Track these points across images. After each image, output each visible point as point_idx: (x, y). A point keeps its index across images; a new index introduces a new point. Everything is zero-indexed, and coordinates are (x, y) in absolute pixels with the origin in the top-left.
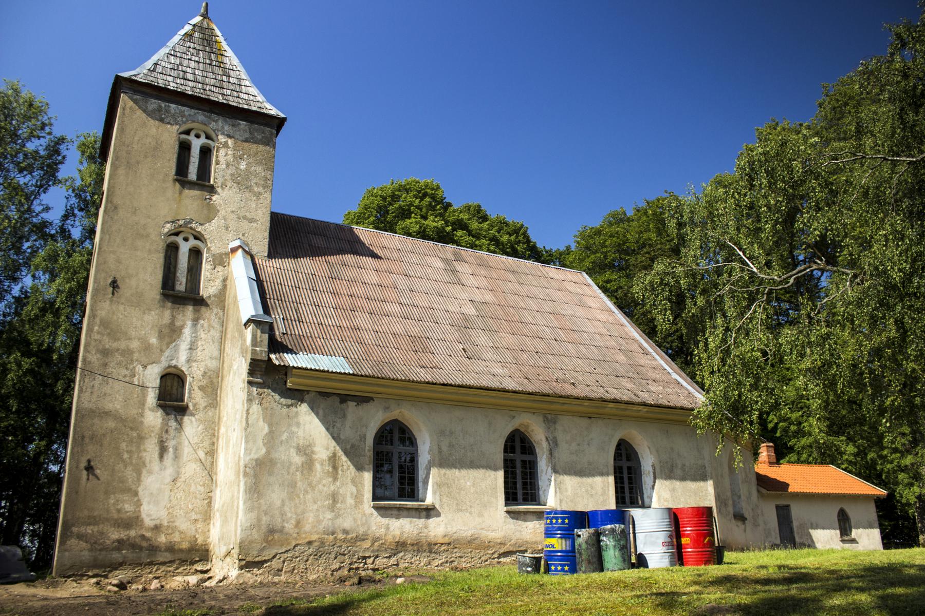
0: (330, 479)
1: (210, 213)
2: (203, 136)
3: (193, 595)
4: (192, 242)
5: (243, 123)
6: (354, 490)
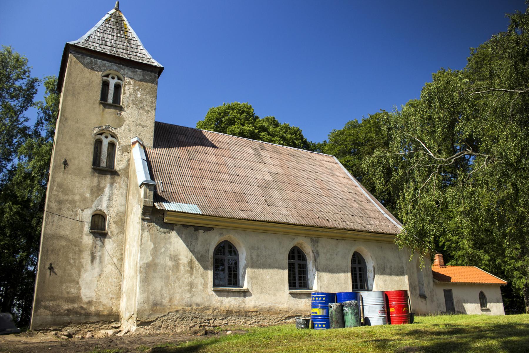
0: (189, 275)
1: (120, 122)
2: (116, 78)
4: (110, 139)
5: (139, 71)
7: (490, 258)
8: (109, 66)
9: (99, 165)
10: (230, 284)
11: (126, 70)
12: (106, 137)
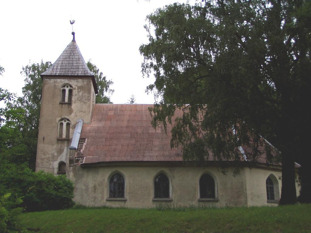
0: (94, 193)
1: (71, 112)
2: (69, 87)
3: (276, 87)
4: (67, 122)
5: (80, 80)
6: (101, 195)
7: (62, 178)
8: (63, 81)
9: (62, 137)
10: (119, 196)
11: (73, 82)
12: (65, 121)
